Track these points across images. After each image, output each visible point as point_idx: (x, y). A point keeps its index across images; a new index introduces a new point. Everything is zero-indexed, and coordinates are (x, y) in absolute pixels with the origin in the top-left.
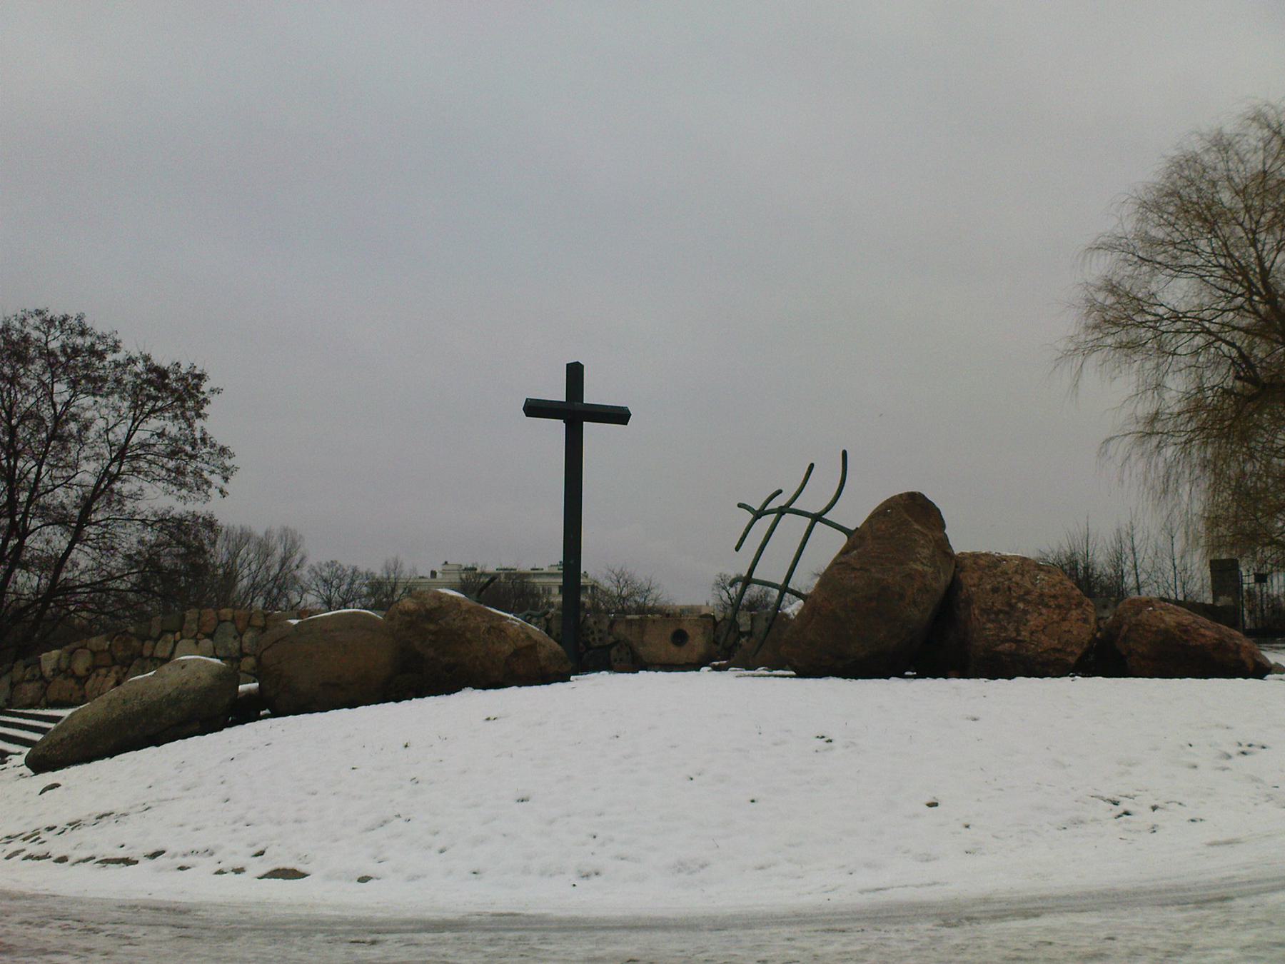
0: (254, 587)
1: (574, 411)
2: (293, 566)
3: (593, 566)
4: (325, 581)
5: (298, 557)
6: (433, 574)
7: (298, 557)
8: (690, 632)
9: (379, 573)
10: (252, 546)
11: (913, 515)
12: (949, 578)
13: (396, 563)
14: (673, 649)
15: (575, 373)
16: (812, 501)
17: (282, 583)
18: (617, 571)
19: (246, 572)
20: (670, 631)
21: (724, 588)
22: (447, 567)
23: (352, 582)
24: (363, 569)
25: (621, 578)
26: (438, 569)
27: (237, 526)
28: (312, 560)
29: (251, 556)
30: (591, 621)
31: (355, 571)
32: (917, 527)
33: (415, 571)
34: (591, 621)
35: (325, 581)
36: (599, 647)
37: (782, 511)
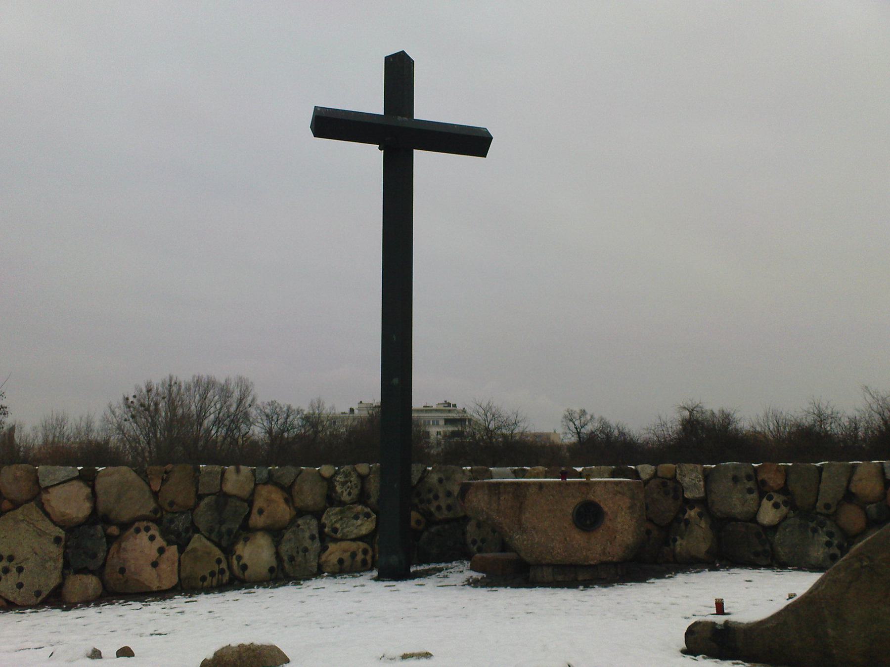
0: (218, 422)
1: (397, 131)
2: (247, 405)
3: (427, 390)
4: (267, 416)
5: (250, 398)
6: (352, 410)
7: (250, 398)
8: (607, 506)
9: (307, 410)
10: (216, 389)
13: (319, 402)
14: (578, 538)
15: (399, 72)
17: (240, 417)
18: (484, 405)
19: (212, 410)
20: (571, 503)
21: (571, 420)
22: (362, 405)
23: (288, 416)
24: (294, 407)
25: (205, 387)
26: (355, 407)
27: (205, 376)
29: (217, 397)
30: (434, 478)
31: (289, 408)
33: (333, 408)
34: (434, 478)
35: (267, 416)
36: (447, 521)
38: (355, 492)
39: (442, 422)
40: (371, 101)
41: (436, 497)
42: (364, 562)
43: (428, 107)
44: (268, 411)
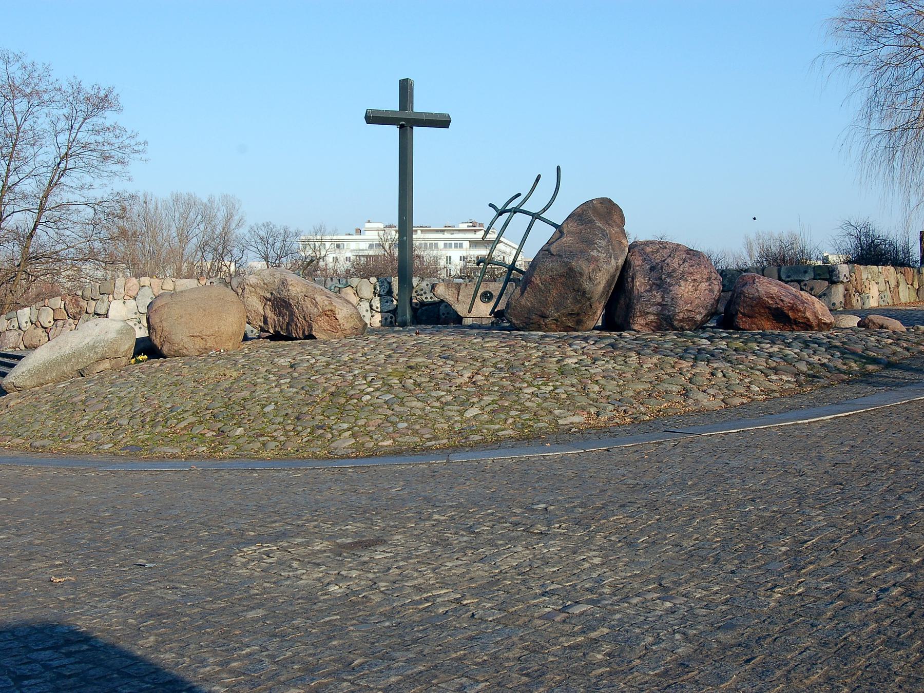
1: (406, 120)
7: (236, 218)
11: (601, 215)
12: (621, 262)
16: (533, 205)
25: (186, 206)
28: (250, 221)
29: (200, 217)
32: (599, 224)
37: (515, 210)
38: (386, 290)
39: (466, 244)
40: (392, 104)
41: (425, 293)
42: (391, 322)
43: (421, 105)
44: (262, 233)
